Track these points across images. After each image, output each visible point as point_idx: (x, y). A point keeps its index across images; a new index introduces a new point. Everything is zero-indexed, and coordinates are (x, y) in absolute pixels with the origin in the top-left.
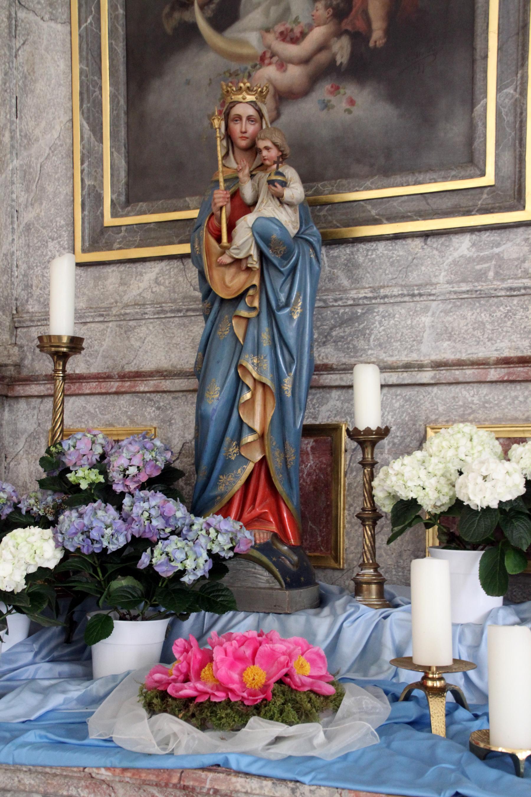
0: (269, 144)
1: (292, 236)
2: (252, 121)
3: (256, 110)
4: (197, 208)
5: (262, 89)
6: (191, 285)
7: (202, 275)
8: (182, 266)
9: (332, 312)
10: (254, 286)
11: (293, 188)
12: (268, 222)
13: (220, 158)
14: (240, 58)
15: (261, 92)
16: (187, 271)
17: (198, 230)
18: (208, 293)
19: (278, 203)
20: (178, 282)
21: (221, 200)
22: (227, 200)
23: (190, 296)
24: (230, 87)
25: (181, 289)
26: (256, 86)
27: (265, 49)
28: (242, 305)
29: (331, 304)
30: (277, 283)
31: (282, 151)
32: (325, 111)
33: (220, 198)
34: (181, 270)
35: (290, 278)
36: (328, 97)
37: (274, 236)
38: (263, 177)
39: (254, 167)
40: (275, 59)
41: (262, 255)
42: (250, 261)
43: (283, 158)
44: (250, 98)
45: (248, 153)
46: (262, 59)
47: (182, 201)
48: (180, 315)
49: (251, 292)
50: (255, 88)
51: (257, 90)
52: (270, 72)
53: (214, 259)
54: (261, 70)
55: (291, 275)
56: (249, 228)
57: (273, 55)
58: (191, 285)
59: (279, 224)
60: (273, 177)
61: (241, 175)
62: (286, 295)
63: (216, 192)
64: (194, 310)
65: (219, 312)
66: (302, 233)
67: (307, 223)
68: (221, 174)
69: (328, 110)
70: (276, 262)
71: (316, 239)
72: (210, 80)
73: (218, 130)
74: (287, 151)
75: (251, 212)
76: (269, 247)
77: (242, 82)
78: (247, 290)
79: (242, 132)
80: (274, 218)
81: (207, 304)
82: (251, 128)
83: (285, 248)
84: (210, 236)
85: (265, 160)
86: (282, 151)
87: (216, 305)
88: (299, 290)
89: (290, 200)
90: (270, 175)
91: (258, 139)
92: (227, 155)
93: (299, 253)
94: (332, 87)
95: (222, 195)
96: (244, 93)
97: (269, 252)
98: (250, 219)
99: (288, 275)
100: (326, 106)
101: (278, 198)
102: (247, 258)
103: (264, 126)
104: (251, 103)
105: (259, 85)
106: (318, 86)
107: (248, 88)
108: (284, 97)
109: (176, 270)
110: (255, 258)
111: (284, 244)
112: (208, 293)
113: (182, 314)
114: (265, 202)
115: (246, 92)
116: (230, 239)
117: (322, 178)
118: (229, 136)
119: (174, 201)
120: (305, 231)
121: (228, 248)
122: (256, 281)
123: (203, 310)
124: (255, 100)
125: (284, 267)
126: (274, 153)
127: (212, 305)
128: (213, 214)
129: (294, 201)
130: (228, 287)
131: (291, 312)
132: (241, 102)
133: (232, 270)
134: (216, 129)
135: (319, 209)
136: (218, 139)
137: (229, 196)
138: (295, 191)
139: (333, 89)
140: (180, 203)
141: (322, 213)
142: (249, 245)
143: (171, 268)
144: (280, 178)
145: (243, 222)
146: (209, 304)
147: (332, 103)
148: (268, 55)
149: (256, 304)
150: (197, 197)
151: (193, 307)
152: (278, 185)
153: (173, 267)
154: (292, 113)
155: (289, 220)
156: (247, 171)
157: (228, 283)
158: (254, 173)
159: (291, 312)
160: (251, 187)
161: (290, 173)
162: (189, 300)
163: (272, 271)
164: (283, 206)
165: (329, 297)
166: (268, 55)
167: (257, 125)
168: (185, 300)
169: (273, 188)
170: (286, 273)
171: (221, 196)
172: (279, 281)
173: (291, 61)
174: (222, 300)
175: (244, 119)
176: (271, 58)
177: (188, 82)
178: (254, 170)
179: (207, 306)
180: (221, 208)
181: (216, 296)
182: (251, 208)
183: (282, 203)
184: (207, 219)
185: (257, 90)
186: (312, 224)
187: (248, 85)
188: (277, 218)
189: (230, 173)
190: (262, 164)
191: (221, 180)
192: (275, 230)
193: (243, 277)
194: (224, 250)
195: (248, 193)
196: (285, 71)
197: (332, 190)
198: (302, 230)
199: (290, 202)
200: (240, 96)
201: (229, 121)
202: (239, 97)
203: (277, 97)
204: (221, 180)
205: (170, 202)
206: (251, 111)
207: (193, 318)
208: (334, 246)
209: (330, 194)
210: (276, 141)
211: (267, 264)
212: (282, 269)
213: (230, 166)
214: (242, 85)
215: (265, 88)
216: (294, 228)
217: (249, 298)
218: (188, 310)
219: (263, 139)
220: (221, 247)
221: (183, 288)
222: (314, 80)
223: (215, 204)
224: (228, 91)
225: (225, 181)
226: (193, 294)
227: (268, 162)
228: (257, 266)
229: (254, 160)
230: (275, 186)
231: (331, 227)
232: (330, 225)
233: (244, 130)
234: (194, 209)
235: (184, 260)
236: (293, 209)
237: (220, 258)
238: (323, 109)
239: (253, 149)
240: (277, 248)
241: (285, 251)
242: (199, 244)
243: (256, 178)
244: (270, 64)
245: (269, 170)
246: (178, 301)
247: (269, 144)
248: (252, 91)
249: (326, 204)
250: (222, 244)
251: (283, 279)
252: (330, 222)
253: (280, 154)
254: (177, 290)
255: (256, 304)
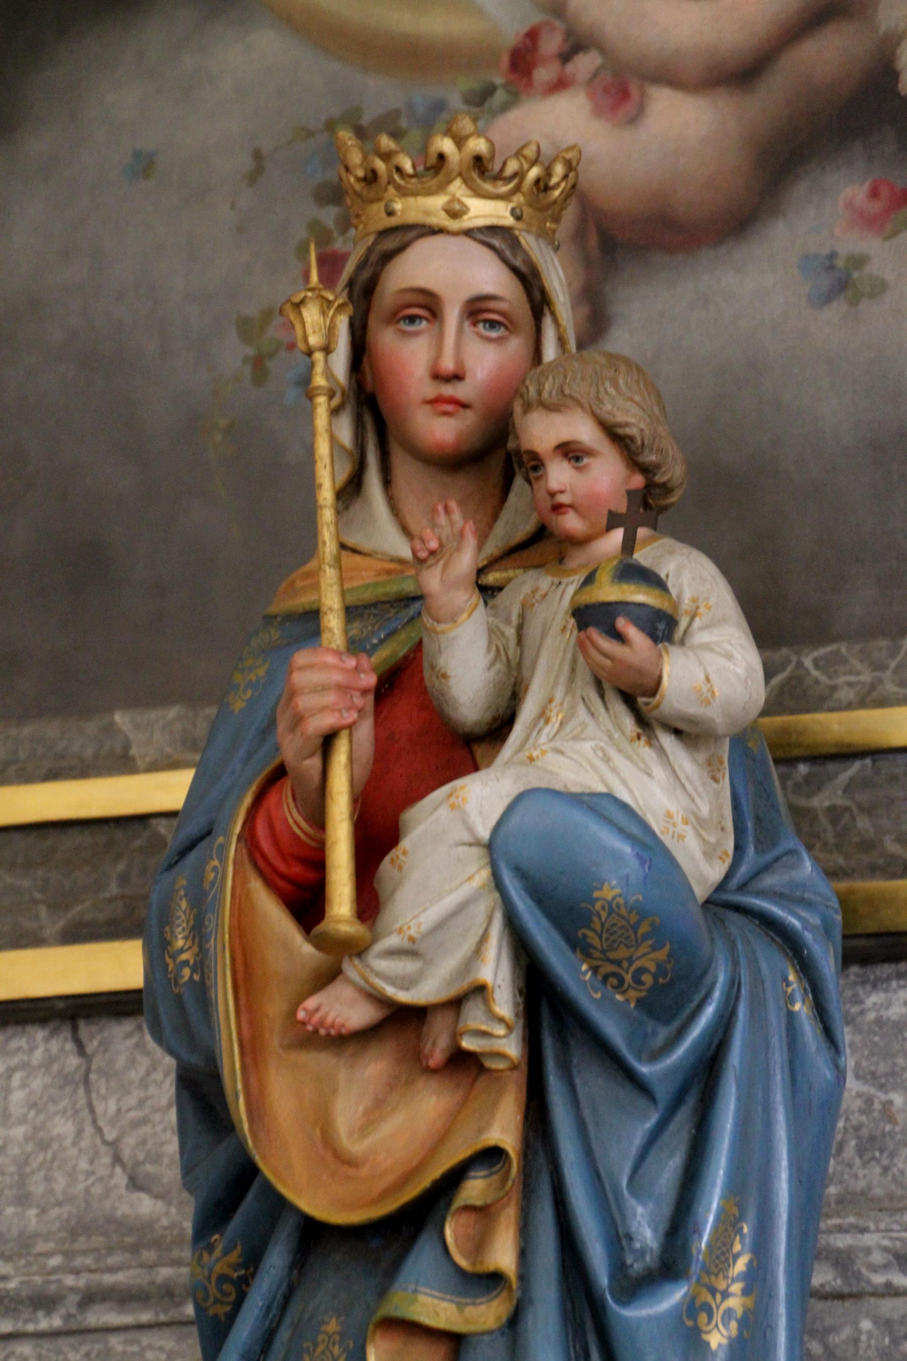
0: (583, 431)
1: (701, 893)
2: (493, 324)
3: (515, 271)
4: (174, 765)
5: (548, 172)
6: (117, 1159)
7: (203, 1097)
8: (74, 1061)
9: (886, 1325)
10: (492, 1155)
11: (707, 647)
12: (578, 817)
13: (326, 495)
14: (411, 57)
15: (542, 185)
16: (101, 1085)
17: (193, 856)
18: (233, 1191)
19: (628, 723)
20: (43, 1146)
21: (330, 698)
22: (358, 701)
23: (110, 1220)
24: (386, 156)
25: (60, 1183)
26: (518, 154)
27: (536, 18)
28: (422, 1259)
29: (879, 1279)
30: (616, 1146)
31: (646, 470)
32: (838, 308)
33: (324, 688)
34: (66, 1079)
35: (684, 1117)
36: (850, 242)
37: (611, 890)
38: (550, 597)
39: (492, 548)
40: (585, 64)
41: (539, 992)
42: (473, 1016)
43: (649, 504)
44: (483, 211)
45: (463, 482)
46: (522, 61)
47: (91, 727)
48: (44, 1323)
49: (475, 1189)
50: (512, 166)
51: (519, 175)
52: (559, 121)
53: (274, 1008)
54: (514, 115)
55: (691, 1101)
56: (476, 843)
57: (576, 44)
58: (117, 1159)
59: (634, 829)
60: (609, 591)
61: (433, 581)
62: (667, 1211)
63: (302, 657)
64: (124, 1298)
65: (287, 1299)
66: (742, 887)
67: (767, 837)
68: (329, 575)
69: (854, 302)
70: (613, 1030)
71: (815, 920)
72: (257, 155)
73: (319, 356)
74: (674, 471)
75: (476, 768)
76: (578, 945)
77: (448, 132)
78: (455, 1178)
79: (438, 377)
80: (610, 797)
81: (223, 1258)
82: (486, 361)
83: (661, 955)
84: (257, 886)
85: (558, 508)
86: (646, 470)
87: (277, 1260)
88: (736, 1189)
89: (694, 709)
90: (589, 580)
91: (528, 407)
92: (351, 490)
93: (734, 985)
94: (874, 193)
95: (337, 677)
96: (457, 188)
97: (573, 975)
98: (481, 797)
99: (678, 1101)
100: (841, 282)
101: (629, 700)
102: (456, 1004)
103: (550, 352)
104: (488, 236)
105: (530, 152)
106: (800, 190)
107: (478, 160)
108: (624, 240)
109: (37, 1083)
110: (504, 1002)
111: (658, 935)
112: (233, 1191)
113: (56, 1322)
114: (555, 720)
115: (467, 182)
116: (369, 903)
117: (819, 632)
118: (369, 400)
119: (51, 729)
120: (757, 874)
121: (356, 949)
122: (504, 1129)
123: (198, 1293)
124: (509, 221)
125: (654, 1057)
126: (606, 477)
127: (253, 1260)
128: (280, 773)
129: (714, 714)
130: (350, 1162)
131: (694, 1309)
132: (438, 231)
133: (375, 1067)
134: (309, 353)
135: (807, 779)
136: (322, 400)
137: (370, 680)
138: (717, 664)
139: (874, 207)
140: (81, 737)
141: (821, 801)
142: (467, 947)
143: (11, 1071)
144: (640, 595)
145: (443, 812)
146: (235, 1257)
147: (873, 268)
148: (551, 44)
149: (503, 1256)
150: (173, 712)
151: (120, 1277)
152: (633, 633)
153: (25, 1066)
154: (660, 313)
155: (680, 808)
156: (466, 560)
157: (349, 1134)
158: (492, 578)
159: (694, 1309)
160: (482, 642)
161: (692, 576)
162: (98, 1241)
163: (594, 1082)
164: (652, 740)
165: (870, 1239)
166: (551, 44)
167: (516, 345)
168: (81, 1243)
169: (606, 644)
170: (663, 1093)
171: (327, 682)
172: (626, 1131)
173: (668, 75)
174: (313, 1235)
175: (452, 315)
176: (565, 58)
177: (144, 166)
178: (493, 563)
179: (219, 1268)
180: (328, 742)
181: (278, 1205)
182: (479, 751)
183: (645, 723)
184: (248, 800)
185: (519, 175)
186: (790, 841)
187: (478, 145)
188: (626, 798)
189: (367, 577)
190: (541, 534)
191: (331, 601)
192: (618, 857)
193: (430, 1103)
194: (338, 955)
195: (466, 672)
196: (634, 120)
197: (873, 687)
198: (744, 870)
199: (692, 720)
200: (437, 202)
201: (373, 321)
202: (431, 207)
203: (593, 240)
204: (331, 601)
205: (28, 730)
206: (488, 276)
207: (116, 1342)
208: (887, 969)
209: (863, 703)
210: (620, 418)
211: (563, 1042)
212: (644, 1069)
213: (366, 546)
214: (447, 145)
215: (559, 170)
216: (709, 853)
217: (467, 1219)
218: (89, 1298)
219: (551, 408)
220: (323, 943)
221: (72, 1175)
222: (781, 163)
223: (298, 720)
224: (372, 178)
225: (351, 612)
226: (123, 1210)
227: (572, 523)
228: (512, 1047)
229: (495, 516)
230: (620, 637)
231: (874, 870)
232: (866, 859)
233: (446, 368)
234: (155, 767)
235: (85, 1030)
236: (702, 757)
237: (311, 1003)
238: (827, 298)
239: (494, 459)
240: (621, 953)
241: (661, 970)
242: (198, 932)
243: (511, 600)
244: (560, 85)
245: (577, 559)
246: (42, 1247)
247: (583, 431)
248: (499, 177)
249: (847, 754)
250: (324, 926)
251: (650, 1124)
252: (867, 845)
253: (638, 481)
254: (37, 1188)
255: (503, 1256)
